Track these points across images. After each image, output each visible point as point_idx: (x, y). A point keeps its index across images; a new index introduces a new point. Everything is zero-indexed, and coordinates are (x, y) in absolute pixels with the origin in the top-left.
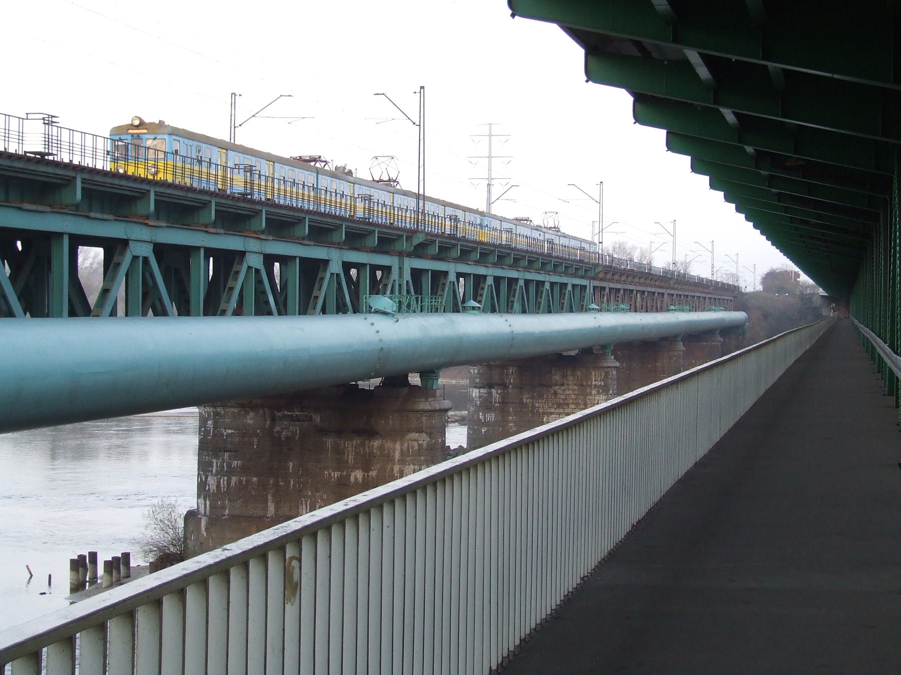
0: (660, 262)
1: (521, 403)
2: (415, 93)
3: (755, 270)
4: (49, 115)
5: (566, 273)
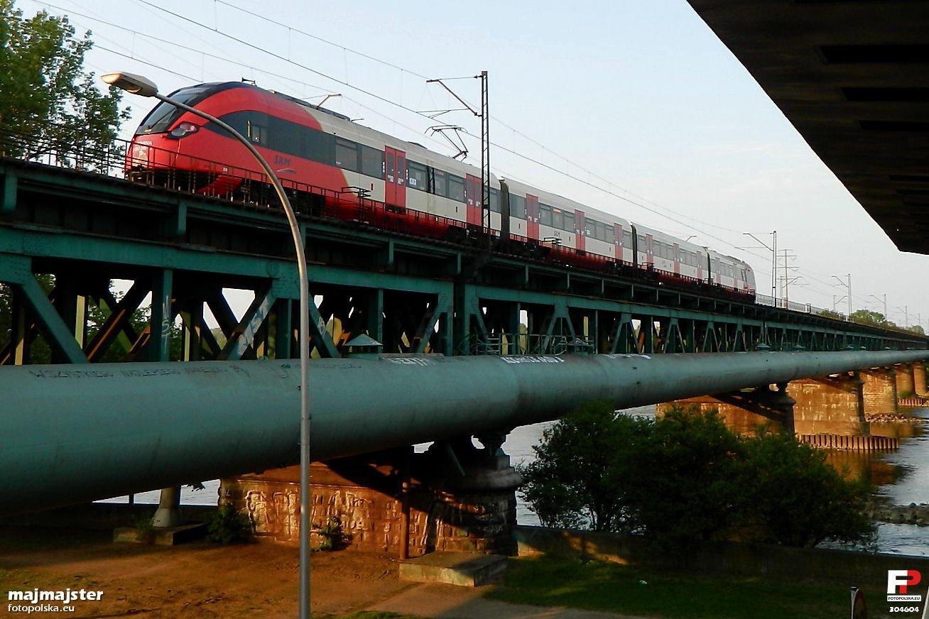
0: (845, 310)
2: (476, 77)
3: (485, 104)
4: (360, 189)
5: (780, 321)
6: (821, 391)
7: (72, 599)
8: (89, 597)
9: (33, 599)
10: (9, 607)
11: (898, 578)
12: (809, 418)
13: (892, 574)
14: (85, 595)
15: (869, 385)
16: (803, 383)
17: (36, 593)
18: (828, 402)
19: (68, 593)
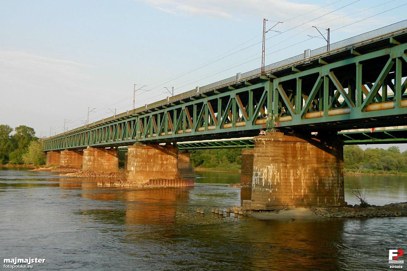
1: (98, 160)
2: (267, 20)
6: (157, 154)
7: (32, 262)
8: (39, 261)
9: (15, 262)
10: (4, 266)
11: (394, 253)
12: (151, 169)
13: (391, 251)
14: (37, 260)
15: (106, 158)
16: (148, 149)
17: (16, 260)
18: (162, 160)
19: (30, 260)
